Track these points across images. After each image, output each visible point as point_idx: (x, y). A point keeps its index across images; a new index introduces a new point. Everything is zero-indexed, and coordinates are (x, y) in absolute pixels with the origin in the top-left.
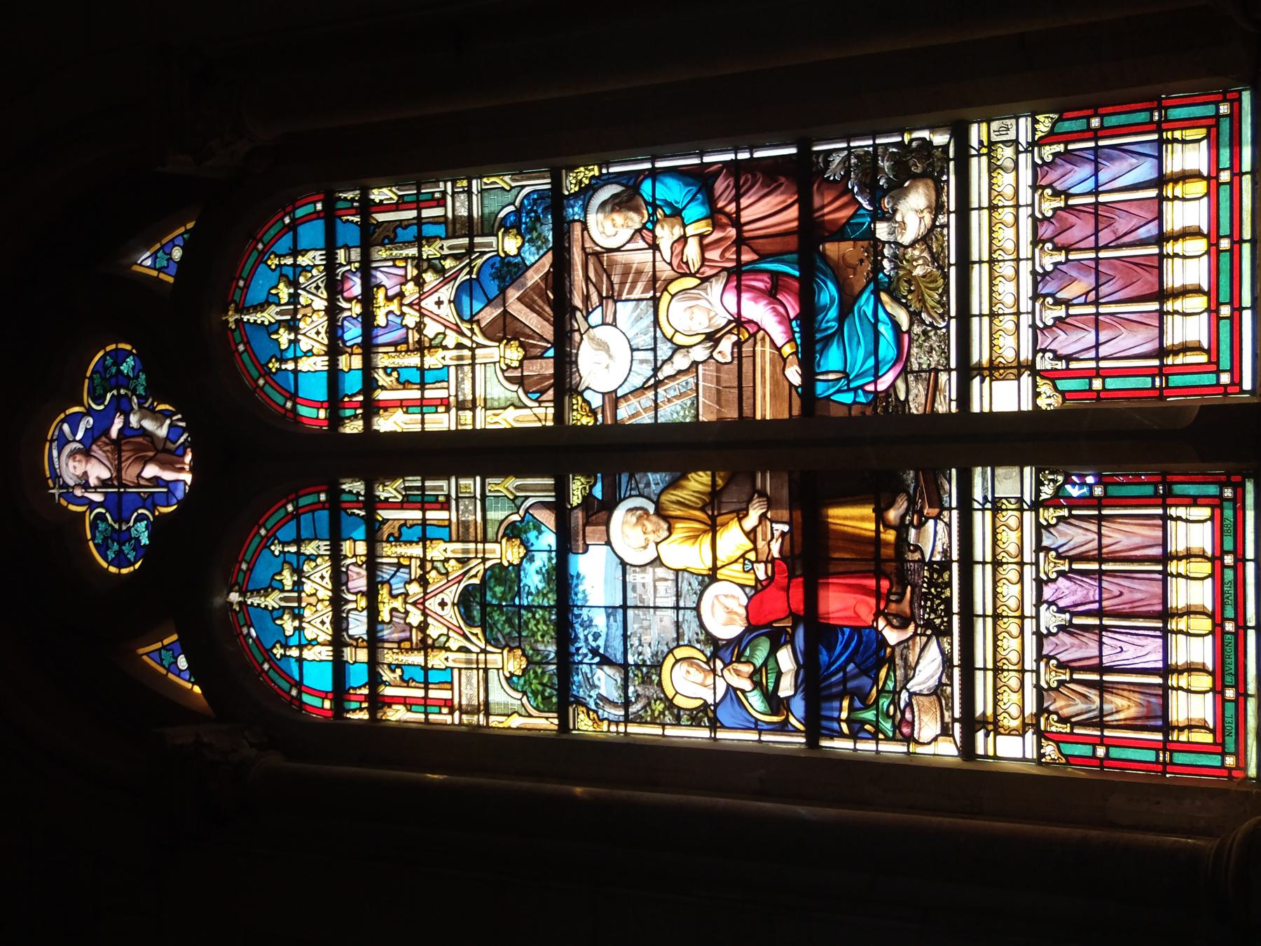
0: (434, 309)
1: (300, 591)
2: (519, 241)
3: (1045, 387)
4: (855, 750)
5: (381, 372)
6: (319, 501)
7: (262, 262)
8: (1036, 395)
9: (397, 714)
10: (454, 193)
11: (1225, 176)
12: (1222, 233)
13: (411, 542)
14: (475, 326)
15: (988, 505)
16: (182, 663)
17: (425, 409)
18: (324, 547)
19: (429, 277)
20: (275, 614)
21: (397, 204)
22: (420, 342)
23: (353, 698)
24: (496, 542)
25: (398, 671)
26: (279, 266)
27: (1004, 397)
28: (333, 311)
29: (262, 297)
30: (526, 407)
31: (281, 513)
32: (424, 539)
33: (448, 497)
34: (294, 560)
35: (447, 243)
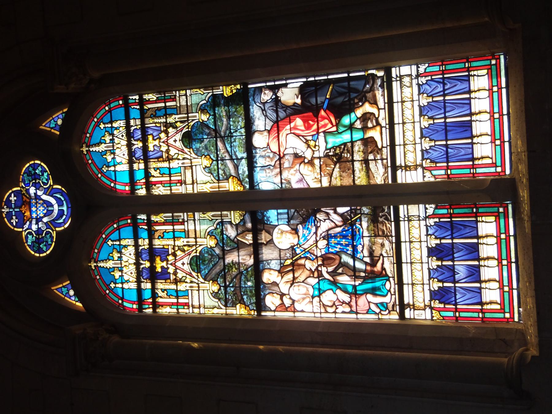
0: (173, 143)
1: (113, 143)
2: (208, 116)
3: (428, 174)
4: (357, 318)
5: (153, 170)
6: (119, 104)
7: (97, 126)
8: (424, 177)
9: (165, 311)
10: (180, 96)
11: (495, 89)
12: (496, 138)
13: (160, 117)
14: (199, 274)
15: (406, 219)
16: (72, 293)
17: (179, 307)
18: (131, 242)
19: (171, 130)
20: (103, 154)
21: (164, 223)
22: (175, 279)
23: (146, 303)
24: (197, 112)
25: (166, 292)
26: (105, 127)
27: (413, 177)
28: (129, 145)
29: (98, 141)
30: (221, 308)
31: (104, 111)
32: (174, 238)
33: (183, 219)
34: (110, 130)
35: (177, 116)
